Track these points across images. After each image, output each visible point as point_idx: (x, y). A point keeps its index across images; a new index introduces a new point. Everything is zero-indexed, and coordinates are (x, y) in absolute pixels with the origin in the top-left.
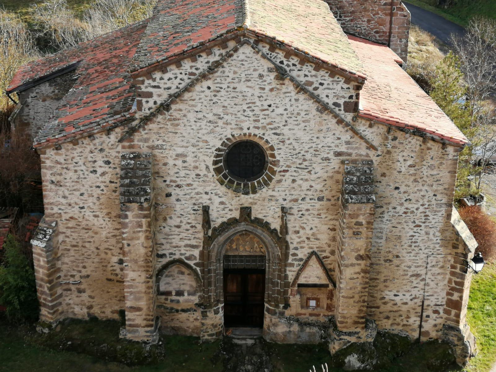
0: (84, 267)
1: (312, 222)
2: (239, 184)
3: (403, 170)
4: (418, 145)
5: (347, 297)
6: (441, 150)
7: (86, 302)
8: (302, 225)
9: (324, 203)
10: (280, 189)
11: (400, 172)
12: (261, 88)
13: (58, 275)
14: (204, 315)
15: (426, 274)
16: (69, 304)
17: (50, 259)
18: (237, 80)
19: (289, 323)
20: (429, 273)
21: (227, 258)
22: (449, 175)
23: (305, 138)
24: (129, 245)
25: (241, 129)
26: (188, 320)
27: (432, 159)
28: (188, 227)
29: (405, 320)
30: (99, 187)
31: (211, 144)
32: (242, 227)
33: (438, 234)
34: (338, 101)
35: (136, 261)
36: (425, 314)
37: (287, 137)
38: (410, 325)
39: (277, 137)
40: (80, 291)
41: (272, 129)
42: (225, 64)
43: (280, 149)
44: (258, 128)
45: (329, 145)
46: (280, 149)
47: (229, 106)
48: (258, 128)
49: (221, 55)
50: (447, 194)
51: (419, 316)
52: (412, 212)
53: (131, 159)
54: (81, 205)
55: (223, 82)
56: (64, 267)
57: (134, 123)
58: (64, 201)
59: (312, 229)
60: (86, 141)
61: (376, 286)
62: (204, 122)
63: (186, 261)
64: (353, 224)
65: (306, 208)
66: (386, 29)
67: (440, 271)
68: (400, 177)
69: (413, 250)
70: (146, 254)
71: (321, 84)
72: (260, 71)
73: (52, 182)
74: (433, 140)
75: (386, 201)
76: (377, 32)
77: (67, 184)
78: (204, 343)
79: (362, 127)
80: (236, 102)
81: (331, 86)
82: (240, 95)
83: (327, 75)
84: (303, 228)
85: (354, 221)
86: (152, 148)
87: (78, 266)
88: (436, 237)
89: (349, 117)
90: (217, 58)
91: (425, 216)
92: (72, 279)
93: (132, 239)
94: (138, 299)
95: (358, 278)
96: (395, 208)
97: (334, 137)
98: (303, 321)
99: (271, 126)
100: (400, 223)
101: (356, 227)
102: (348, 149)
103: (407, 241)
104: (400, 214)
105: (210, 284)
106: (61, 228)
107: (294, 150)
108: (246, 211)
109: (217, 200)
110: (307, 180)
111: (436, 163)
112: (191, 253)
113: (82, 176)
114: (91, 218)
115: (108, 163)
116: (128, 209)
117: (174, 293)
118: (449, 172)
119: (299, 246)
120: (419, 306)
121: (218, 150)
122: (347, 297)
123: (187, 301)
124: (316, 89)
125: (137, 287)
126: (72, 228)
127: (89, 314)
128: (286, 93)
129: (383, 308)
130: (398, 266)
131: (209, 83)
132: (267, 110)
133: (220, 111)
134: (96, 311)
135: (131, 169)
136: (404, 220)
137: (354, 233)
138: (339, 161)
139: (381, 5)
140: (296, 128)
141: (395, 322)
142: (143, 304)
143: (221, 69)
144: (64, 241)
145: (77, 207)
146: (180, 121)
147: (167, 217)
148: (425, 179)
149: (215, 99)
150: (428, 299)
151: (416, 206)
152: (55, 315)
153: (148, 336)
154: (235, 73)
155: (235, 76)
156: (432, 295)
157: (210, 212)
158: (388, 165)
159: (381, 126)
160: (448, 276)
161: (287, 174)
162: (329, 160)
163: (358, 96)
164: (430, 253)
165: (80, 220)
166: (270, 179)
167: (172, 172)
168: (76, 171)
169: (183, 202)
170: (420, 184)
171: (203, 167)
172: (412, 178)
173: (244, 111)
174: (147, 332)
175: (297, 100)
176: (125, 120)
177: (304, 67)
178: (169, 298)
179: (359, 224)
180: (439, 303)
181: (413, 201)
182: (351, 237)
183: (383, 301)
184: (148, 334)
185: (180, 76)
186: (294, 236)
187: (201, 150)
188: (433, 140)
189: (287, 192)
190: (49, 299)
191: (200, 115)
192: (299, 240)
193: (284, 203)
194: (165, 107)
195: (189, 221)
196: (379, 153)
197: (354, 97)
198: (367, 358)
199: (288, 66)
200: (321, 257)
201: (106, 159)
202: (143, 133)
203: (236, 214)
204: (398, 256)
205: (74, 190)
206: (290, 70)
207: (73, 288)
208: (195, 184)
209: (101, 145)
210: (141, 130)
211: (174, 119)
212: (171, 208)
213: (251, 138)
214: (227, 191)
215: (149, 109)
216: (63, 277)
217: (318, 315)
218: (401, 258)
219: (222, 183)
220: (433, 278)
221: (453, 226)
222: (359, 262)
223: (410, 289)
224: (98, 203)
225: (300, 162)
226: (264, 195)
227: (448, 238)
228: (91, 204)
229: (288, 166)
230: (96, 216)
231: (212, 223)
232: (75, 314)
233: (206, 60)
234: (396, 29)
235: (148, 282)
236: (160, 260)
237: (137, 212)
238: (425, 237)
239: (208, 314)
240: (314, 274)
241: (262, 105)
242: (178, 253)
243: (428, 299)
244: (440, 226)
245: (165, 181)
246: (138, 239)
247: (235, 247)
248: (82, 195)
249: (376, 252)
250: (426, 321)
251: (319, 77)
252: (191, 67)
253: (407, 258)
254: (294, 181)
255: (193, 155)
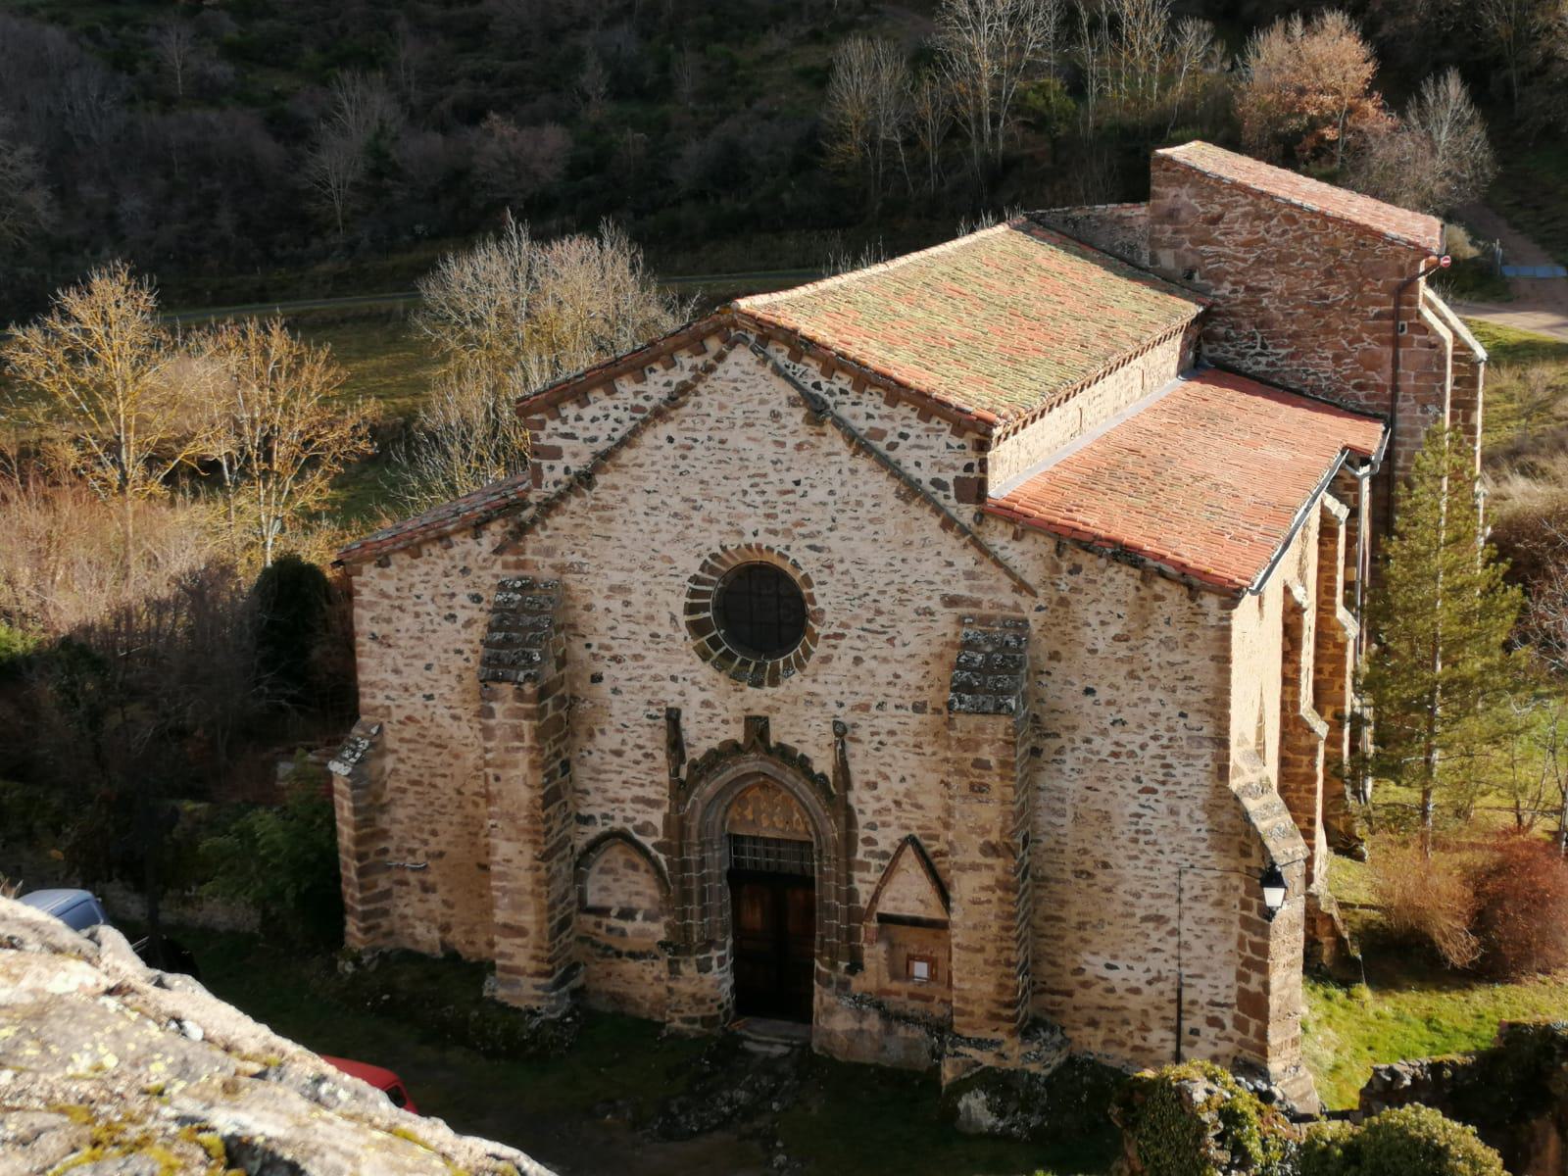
0: (434, 833)
1: (902, 763)
2: (745, 664)
3: (1101, 646)
4: (1131, 589)
5: (967, 948)
6: (1187, 603)
7: (437, 913)
8: (883, 769)
9: (927, 717)
10: (829, 678)
11: (1093, 651)
12: (776, 443)
13: (383, 845)
14: (674, 971)
15: (1180, 917)
16: (404, 917)
17: (361, 804)
18: (726, 423)
19: (859, 1009)
20: (1187, 915)
21: (736, 841)
22: (1212, 665)
23: (878, 560)
24: (497, 779)
25: (740, 533)
26: (642, 978)
27: (1168, 623)
28: (638, 754)
29: (1137, 1034)
30: (459, 652)
31: (680, 565)
32: (751, 764)
33: (1200, 815)
34: (943, 477)
35: (512, 819)
36: (1186, 1025)
37: (837, 557)
38: (1151, 1051)
39: (817, 555)
40: (427, 888)
41: (804, 536)
42: (700, 387)
43: (824, 583)
44: (774, 532)
45: (930, 578)
46: (824, 583)
47: (712, 482)
48: (774, 532)
49: (694, 368)
50: (1211, 715)
51: (1171, 1029)
52: (1132, 754)
53: (515, 590)
54: (428, 692)
55: (699, 426)
56: (396, 830)
57: (527, 514)
58: (394, 679)
59: (903, 780)
60: (436, 550)
61: (1060, 938)
62: (664, 516)
63: (637, 837)
64: (969, 764)
65: (889, 727)
66: (1382, 378)
67: (1215, 913)
68: (1093, 662)
69: (1143, 851)
70: (532, 801)
71: (904, 436)
72: (773, 405)
73: (374, 637)
74: (1162, 574)
75: (1066, 721)
76: (1360, 387)
77: (402, 643)
78: (671, 1036)
79: (998, 538)
80: (727, 473)
81: (924, 442)
82: (735, 456)
83: (914, 415)
84: (886, 778)
85: (970, 756)
86: (562, 569)
87: (421, 830)
88: (1195, 824)
89: (966, 513)
90: (687, 376)
91: (1165, 766)
92: (410, 859)
93: (503, 766)
94: (518, 907)
95: (989, 901)
96: (1088, 741)
97: (939, 563)
98: (893, 1009)
99: (802, 530)
100: (1103, 779)
101: (977, 772)
102: (971, 589)
103: (1125, 828)
104: (1103, 756)
105: (686, 897)
106: (390, 741)
107: (855, 586)
108: (758, 727)
109: (696, 697)
110: (885, 660)
111: (1177, 633)
112: (647, 818)
113: (428, 627)
114: (447, 721)
115: (477, 599)
116: (494, 696)
117: (613, 913)
118: (1213, 658)
119: (877, 820)
120: (1171, 1001)
121: (695, 579)
122: (967, 948)
123: (642, 933)
124: (892, 446)
125: (516, 879)
126: (410, 741)
127: (444, 945)
128: (829, 454)
129: (1081, 997)
130: (1108, 890)
131: (670, 429)
132: (792, 492)
133: (693, 491)
134: (457, 937)
135: (513, 611)
136: (1113, 774)
137: (972, 786)
138: (952, 618)
139: (1367, 318)
140: (856, 535)
141: (1112, 1036)
142: (528, 919)
143: (693, 399)
144: (395, 771)
145: (420, 694)
146: (616, 512)
147: (596, 729)
148: (1155, 671)
149: (684, 465)
150: (1190, 986)
151: (1139, 740)
152: (370, 936)
153: (540, 998)
154: (722, 407)
155: (724, 414)
156: (1201, 976)
157: (683, 723)
158: (1063, 633)
159: (1041, 539)
160: (1236, 929)
161: (843, 643)
162: (932, 614)
163: (983, 464)
164: (1187, 864)
165: (426, 724)
166: (808, 653)
167: (602, 625)
168: (417, 615)
169: (627, 697)
170: (1145, 684)
171: (666, 618)
172: (1124, 669)
173: (745, 493)
174: (537, 987)
175: (853, 471)
176: (507, 505)
177: (865, 397)
178: (605, 921)
179: (980, 764)
180: (1220, 999)
181: (1132, 726)
182: (965, 797)
183: (1080, 978)
184: (540, 993)
185: (614, 414)
186: (866, 795)
187: (660, 579)
188: (1162, 574)
189: (844, 686)
190: (358, 895)
191: (655, 500)
192: (877, 806)
193: (840, 712)
194: (584, 480)
195: (641, 742)
196: (1042, 602)
197: (976, 468)
198: (1012, 1106)
199: (831, 393)
200: (930, 851)
201: (473, 591)
202: (543, 534)
203: (737, 733)
204: (1106, 865)
205: (415, 657)
206: (836, 404)
207: (412, 878)
208: (650, 656)
209: (465, 558)
210: (538, 528)
211: (604, 508)
212: (603, 708)
213: (767, 558)
214: (717, 675)
215: (556, 483)
216: (393, 854)
217: (928, 999)
218: (1115, 870)
219: (705, 656)
220: (1198, 930)
221: (1237, 799)
222: (990, 861)
223: (1142, 953)
224: (459, 689)
225: (870, 616)
226: (794, 690)
227: (1227, 829)
228: (445, 690)
229: (843, 625)
230: (455, 718)
231: (688, 751)
232: (416, 942)
233: (665, 380)
234: (1409, 380)
235: (538, 869)
236: (583, 829)
237: (511, 703)
238: (1169, 821)
239: (682, 967)
240: (909, 893)
241: (781, 481)
242: (619, 815)
243: (1190, 986)
244: (1204, 794)
245: (589, 646)
246: (515, 765)
247: (750, 817)
248: (428, 667)
249: (1053, 850)
250: (1192, 1044)
251: (898, 419)
252: (636, 394)
253: (1130, 873)
254: (858, 660)
255: (644, 589)
